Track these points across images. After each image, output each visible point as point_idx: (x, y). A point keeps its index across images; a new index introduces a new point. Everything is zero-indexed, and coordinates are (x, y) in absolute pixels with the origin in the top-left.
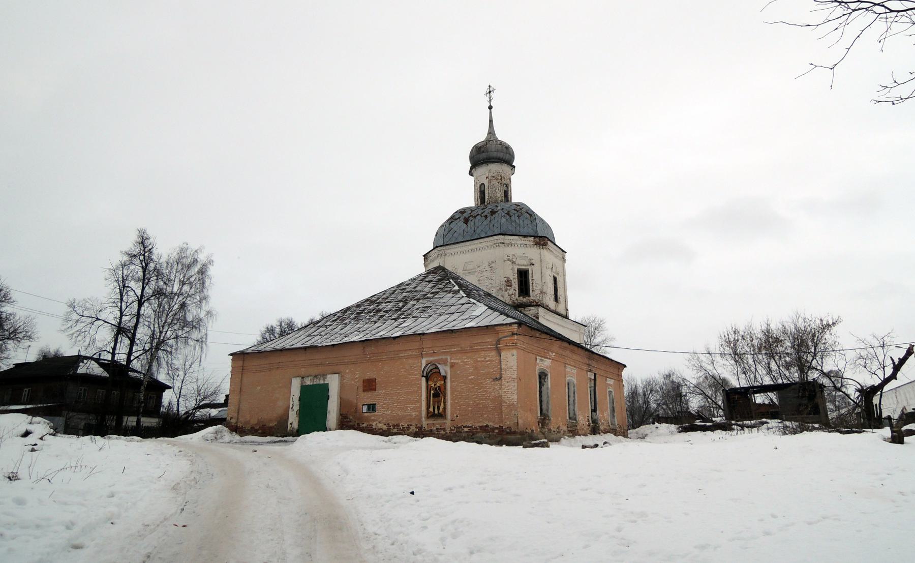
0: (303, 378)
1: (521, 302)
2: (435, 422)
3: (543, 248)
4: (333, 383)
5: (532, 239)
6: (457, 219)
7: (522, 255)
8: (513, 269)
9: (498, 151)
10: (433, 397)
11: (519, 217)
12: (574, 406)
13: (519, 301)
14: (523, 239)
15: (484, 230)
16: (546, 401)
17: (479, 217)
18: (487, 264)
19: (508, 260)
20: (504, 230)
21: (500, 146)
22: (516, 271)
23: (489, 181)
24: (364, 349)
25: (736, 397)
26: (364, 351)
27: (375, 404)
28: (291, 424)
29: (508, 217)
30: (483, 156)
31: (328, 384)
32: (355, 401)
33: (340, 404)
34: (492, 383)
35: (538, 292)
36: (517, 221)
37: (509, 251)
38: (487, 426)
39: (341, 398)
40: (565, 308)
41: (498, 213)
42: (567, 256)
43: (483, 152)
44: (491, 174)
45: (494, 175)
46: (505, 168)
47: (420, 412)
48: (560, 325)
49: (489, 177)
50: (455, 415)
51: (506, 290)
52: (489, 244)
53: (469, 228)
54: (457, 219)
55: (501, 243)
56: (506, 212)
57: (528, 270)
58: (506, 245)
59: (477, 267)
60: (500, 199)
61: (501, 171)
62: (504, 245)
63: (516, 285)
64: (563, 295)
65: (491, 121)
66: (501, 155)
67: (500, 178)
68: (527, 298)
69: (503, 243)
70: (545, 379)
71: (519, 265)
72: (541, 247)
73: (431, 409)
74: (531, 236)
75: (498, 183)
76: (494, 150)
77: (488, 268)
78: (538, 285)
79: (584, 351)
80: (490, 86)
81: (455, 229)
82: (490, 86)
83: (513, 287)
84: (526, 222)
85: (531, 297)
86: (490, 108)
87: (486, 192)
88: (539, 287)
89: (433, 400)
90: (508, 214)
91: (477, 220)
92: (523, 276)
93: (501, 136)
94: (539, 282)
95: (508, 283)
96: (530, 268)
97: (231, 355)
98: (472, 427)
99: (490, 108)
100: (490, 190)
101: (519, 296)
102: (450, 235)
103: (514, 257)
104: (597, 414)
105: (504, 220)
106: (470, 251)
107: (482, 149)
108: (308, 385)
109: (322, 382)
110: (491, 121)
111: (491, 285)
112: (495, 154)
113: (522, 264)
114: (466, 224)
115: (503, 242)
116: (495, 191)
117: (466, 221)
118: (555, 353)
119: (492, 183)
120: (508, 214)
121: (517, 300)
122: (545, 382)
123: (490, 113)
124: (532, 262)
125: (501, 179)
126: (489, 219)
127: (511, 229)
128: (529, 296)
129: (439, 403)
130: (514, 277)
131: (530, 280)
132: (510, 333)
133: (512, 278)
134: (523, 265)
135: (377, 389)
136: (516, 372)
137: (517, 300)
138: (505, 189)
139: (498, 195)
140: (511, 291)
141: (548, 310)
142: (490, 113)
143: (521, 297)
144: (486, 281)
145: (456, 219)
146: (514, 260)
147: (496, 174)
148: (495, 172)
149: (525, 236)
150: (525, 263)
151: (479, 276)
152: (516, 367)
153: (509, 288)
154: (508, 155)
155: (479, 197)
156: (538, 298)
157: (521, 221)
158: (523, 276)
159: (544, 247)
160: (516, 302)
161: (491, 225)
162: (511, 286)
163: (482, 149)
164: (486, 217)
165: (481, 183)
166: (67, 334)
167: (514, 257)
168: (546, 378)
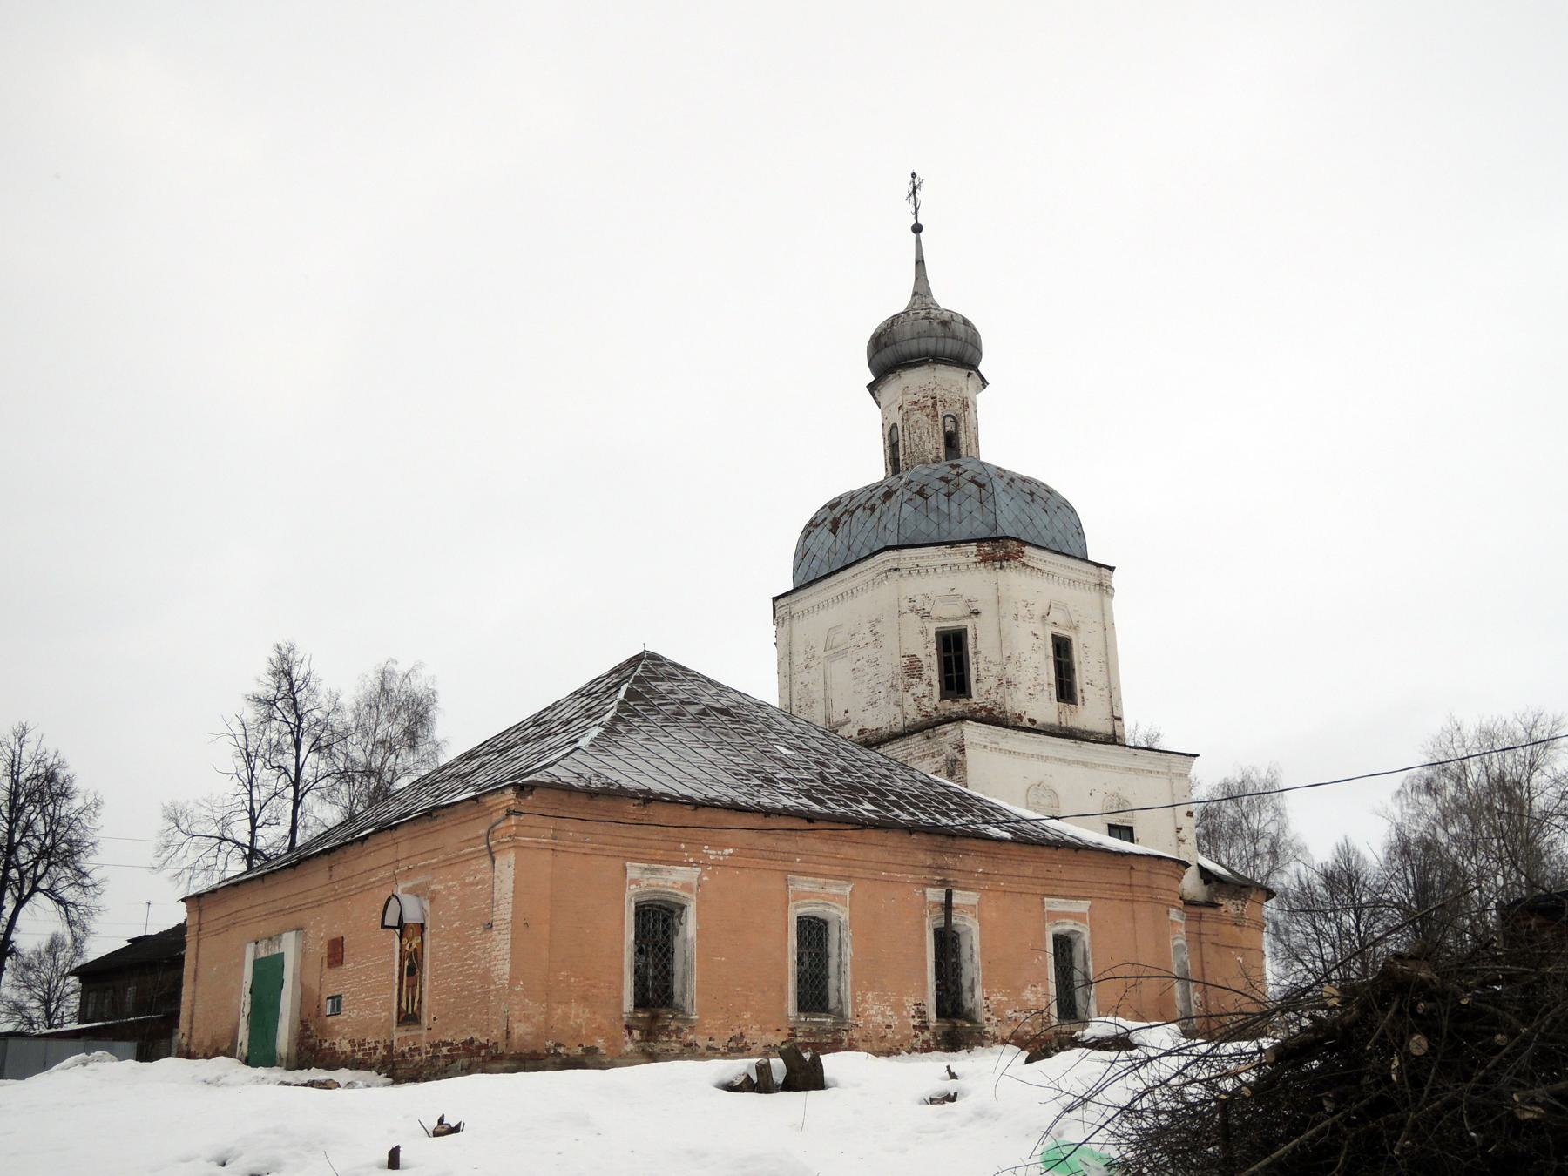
0: (257, 943)
1: (947, 713)
2: (408, 1034)
3: (1002, 567)
4: (289, 946)
5: (973, 548)
6: (820, 523)
7: (947, 592)
8: (924, 632)
9: (919, 336)
10: (408, 975)
11: (948, 495)
12: (839, 980)
13: (942, 712)
14: (948, 551)
15: (866, 543)
16: (682, 970)
17: (859, 511)
18: (866, 629)
19: (912, 611)
20: (908, 534)
21: (926, 322)
22: (932, 636)
23: (903, 415)
24: (330, 870)
25: (1533, 922)
26: (331, 876)
27: (341, 996)
28: (241, 1044)
29: (919, 499)
30: (888, 355)
31: (283, 953)
32: (318, 990)
33: (301, 999)
34: (483, 936)
35: (993, 682)
36: (944, 507)
37: (914, 587)
38: (471, 1041)
39: (302, 985)
40: (1109, 716)
41: (898, 493)
42: (1117, 580)
43: (886, 345)
44: (910, 397)
45: (915, 398)
46: (947, 379)
47: (391, 1013)
48: (1074, 762)
49: (906, 407)
50: (433, 1016)
51: (907, 688)
52: (870, 575)
53: (839, 543)
54: (820, 523)
55: (890, 571)
56: (916, 489)
57: (966, 630)
58: (905, 574)
59: (849, 637)
60: (931, 457)
61: (932, 386)
62: (897, 573)
63: (932, 672)
64: (1101, 681)
65: (920, 262)
66: (929, 345)
67: (930, 403)
68: (963, 701)
69: (896, 569)
70: (681, 916)
71: (940, 619)
72: (998, 564)
73: (404, 1004)
74: (967, 542)
75: (927, 415)
76: (908, 335)
77: (870, 638)
78: (991, 666)
79: (326, 857)
80: (914, 175)
81: (814, 549)
82: (914, 175)
83: (924, 678)
84: (966, 506)
85: (975, 698)
86: (917, 229)
87: (901, 444)
88: (995, 670)
89: (407, 981)
90: (921, 493)
91: (854, 519)
92: (952, 647)
93: (946, 298)
94: (995, 657)
95: (913, 668)
96: (968, 623)
97: (183, 900)
98: (452, 1043)
99: (917, 229)
100: (907, 438)
101: (942, 699)
102: (805, 566)
103: (926, 601)
104: (973, 996)
105: (907, 509)
106: (835, 598)
107: (883, 340)
108: (262, 958)
109: (277, 952)
110: (920, 262)
111: (877, 680)
112: (913, 346)
113: (949, 616)
114: (834, 533)
115: (895, 566)
116: (920, 438)
117: (835, 526)
118: (686, 843)
119: (914, 418)
120: (921, 493)
121: (936, 709)
122: (681, 924)
123: (918, 241)
124: (975, 606)
125: (934, 405)
126: (877, 513)
127: (928, 528)
128: (970, 696)
129: (414, 986)
130: (928, 651)
131: (971, 654)
132: (503, 813)
133: (921, 656)
134: (953, 619)
135: (344, 962)
136: (510, 906)
137: (936, 709)
138: (950, 427)
139: (929, 446)
140: (921, 689)
141: (1028, 730)
142: (918, 241)
143: (948, 701)
144: (867, 670)
145: (817, 526)
146: (928, 609)
147: (921, 394)
148: (917, 390)
149: (952, 544)
150: (959, 613)
151: (855, 661)
152: (512, 894)
153: (914, 681)
154: (950, 341)
155: (888, 461)
156: (993, 697)
157: (954, 506)
158: (952, 647)
159: (1005, 563)
160: (934, 714)
161: (882, 526)
162: (920, 677)
163: (883, 340)
164: (873, 509)
165: (892, 423)
166: (170, 872)
167: (926, 601)
168: (684, 914)
